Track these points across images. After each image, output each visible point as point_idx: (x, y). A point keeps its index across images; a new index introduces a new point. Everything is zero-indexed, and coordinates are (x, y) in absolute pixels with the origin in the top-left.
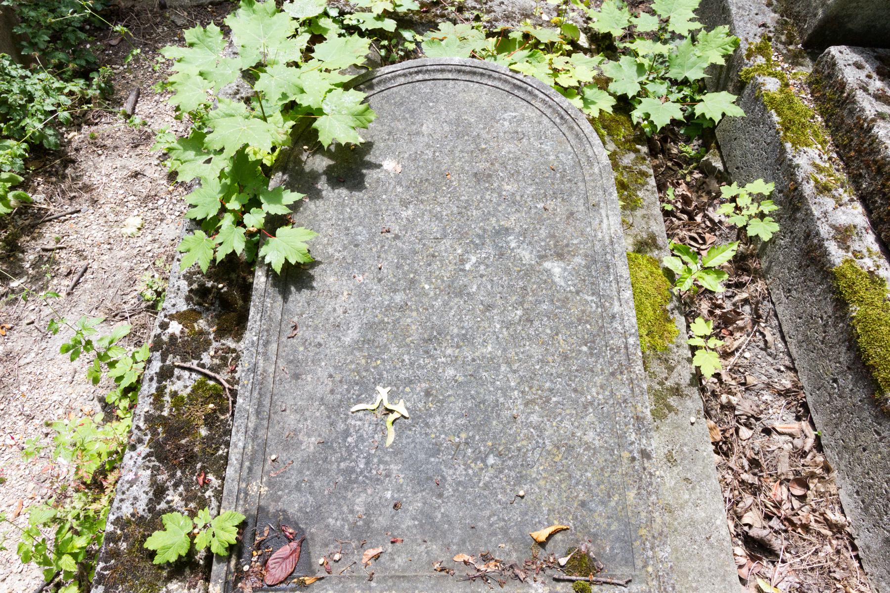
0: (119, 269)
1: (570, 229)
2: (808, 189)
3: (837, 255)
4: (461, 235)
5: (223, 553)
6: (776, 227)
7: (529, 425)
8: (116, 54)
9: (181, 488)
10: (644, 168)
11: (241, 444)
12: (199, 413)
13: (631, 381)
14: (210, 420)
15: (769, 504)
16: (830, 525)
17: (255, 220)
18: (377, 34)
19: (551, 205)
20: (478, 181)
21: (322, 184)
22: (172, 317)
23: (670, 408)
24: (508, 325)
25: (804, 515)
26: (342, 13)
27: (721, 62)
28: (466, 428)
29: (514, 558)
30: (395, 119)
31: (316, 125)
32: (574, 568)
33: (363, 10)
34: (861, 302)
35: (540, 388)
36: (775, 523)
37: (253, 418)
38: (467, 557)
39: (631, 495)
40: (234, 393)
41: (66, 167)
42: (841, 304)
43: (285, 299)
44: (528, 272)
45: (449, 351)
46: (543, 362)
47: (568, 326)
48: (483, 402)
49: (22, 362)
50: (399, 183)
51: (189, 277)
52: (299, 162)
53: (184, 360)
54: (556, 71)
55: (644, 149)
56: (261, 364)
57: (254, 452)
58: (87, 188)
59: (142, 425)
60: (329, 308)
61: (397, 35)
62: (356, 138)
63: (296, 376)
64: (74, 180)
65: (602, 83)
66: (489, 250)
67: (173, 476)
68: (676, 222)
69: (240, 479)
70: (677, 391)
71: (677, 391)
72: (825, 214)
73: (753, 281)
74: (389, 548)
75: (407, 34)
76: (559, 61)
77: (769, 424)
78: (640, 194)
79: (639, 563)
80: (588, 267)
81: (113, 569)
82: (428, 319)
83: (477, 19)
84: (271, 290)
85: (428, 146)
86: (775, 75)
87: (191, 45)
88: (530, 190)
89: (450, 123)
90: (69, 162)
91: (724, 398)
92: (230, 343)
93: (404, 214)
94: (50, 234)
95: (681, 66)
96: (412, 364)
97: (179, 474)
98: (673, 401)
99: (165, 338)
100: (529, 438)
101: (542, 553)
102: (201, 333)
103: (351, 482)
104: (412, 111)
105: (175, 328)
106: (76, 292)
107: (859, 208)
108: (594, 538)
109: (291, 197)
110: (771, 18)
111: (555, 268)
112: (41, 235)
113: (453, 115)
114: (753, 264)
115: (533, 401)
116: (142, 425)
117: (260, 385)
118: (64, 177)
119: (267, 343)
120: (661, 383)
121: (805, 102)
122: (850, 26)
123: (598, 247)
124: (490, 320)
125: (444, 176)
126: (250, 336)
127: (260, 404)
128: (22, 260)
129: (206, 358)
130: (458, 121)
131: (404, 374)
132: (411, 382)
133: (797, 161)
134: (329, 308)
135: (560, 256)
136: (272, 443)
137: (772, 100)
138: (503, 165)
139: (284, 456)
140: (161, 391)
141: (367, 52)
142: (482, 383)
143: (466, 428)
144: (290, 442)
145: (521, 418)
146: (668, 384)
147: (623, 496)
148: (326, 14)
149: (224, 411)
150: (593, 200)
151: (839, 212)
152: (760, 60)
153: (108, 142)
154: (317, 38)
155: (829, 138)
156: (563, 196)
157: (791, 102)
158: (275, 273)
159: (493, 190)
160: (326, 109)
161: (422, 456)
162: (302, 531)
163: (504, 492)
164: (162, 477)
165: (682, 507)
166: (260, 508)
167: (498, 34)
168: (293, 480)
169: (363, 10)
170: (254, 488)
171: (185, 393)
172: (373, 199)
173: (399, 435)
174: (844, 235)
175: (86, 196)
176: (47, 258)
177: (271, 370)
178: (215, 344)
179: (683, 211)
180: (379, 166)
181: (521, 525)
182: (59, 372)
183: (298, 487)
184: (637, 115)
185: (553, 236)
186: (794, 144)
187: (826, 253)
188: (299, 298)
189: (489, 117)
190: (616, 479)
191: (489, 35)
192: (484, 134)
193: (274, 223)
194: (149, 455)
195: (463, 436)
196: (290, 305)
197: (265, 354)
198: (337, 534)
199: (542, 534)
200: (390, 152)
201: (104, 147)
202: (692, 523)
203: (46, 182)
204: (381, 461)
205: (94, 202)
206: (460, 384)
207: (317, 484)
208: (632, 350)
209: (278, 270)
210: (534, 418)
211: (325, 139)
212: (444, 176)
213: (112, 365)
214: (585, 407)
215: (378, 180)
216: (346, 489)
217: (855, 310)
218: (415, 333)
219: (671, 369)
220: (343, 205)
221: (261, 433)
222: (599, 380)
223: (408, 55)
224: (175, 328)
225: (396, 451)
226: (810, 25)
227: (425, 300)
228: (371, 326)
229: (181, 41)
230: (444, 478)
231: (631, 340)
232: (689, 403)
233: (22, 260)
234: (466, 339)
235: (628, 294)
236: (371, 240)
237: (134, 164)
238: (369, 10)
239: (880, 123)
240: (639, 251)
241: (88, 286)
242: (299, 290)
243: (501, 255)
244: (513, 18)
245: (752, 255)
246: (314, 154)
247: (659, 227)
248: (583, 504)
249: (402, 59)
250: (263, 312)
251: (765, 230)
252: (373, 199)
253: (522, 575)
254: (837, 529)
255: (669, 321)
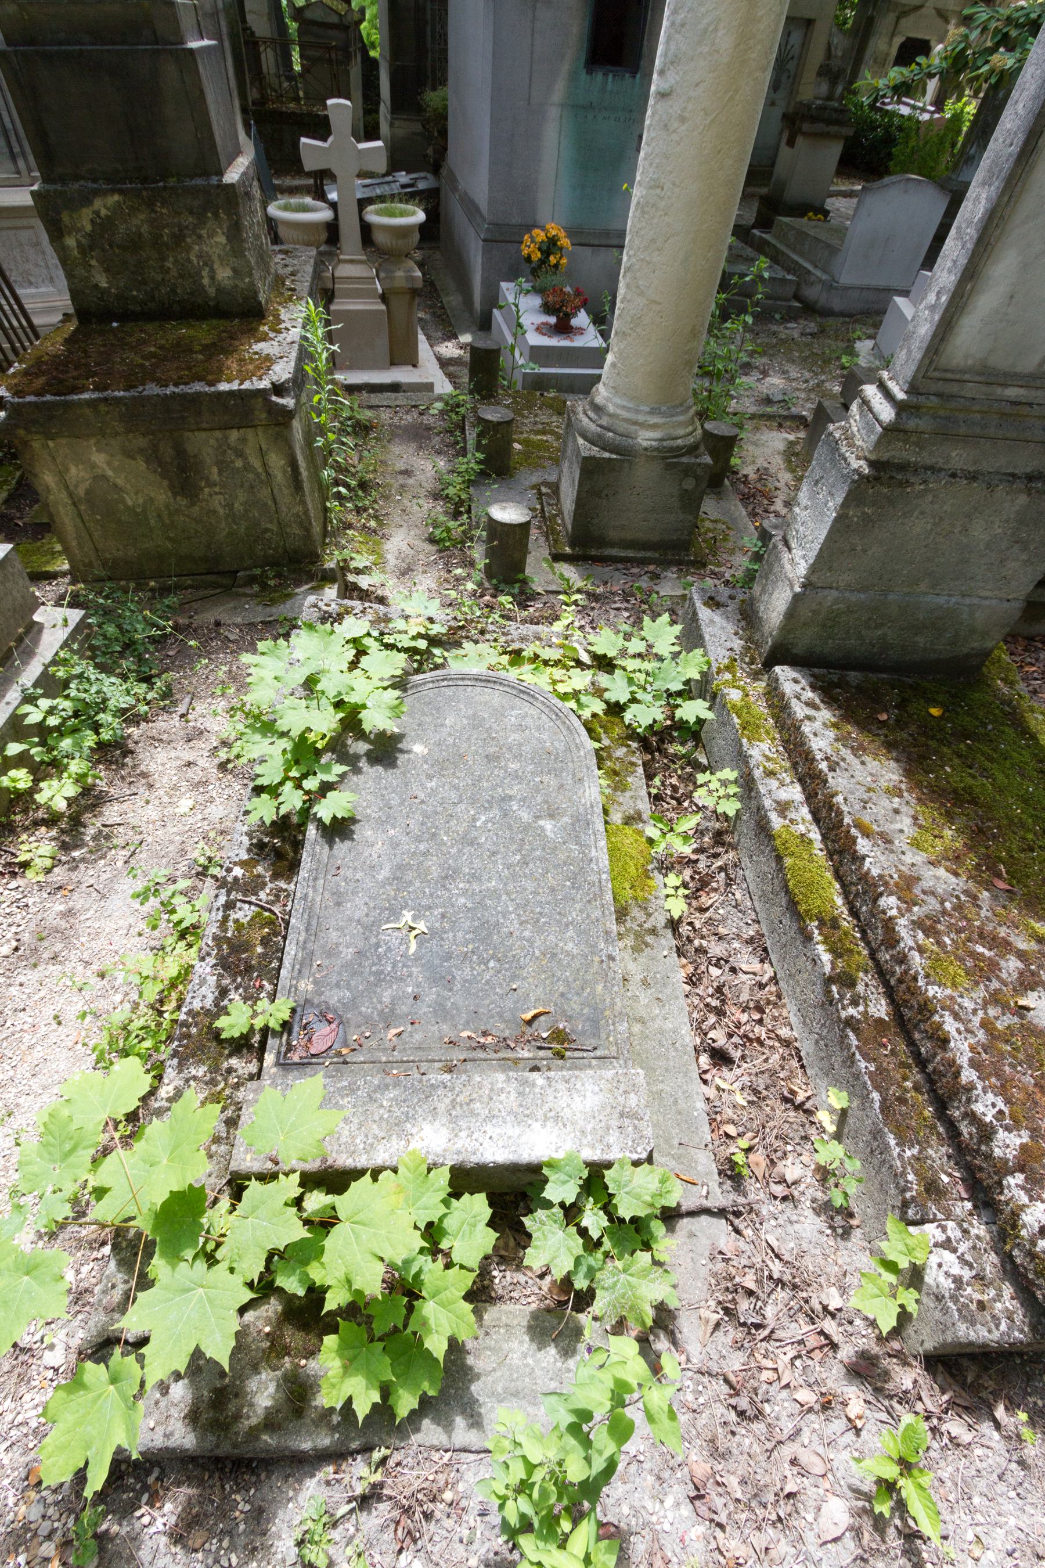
0: (172, 842)
1: (561, 797)
2: (758, 773)
3: (776, 822)
4: (473, 801)
5: (278, 1028)
6: (739, 805)
7: (524, 938)
8: (173, 663)
9: (241, 990)
10: (634, 759)
11: (293, 952)
12: (256, 936)
13: (603, 906)
14: (265, 941)
15: (731, 1025)
16: (779, 1038)
17: (311, 784)
18: (412, 651)
19: (546, 779)
20: (489, 761)
21: (363, 763)
22: (235, 864)
23: (647, 945)
24: (509, 866)
25: (760, 1032)
26: (382, 634)
27: (698, 677)
28: (473, 941)
29: (507, 1033)
30: (424, 714)
31: (360, 716)
32: (554, 1039)
33: (400, 632)
34: (792, 854)
35: (532, 912)
36: (736, 1039)
37: (303, 934)
38: (469, 1033)
39: (599, 988)
40: (287, 923)
41: (125, 757)
42: (779, 859)
43: (331, 848)
44: (526, 828)
45: (461, 885)
46: (535, 893)
47: (556, 867)
48: (487, 922)
49: (82, 918)
50: (426, 762)
51: (250, 834)
52: (346, 746)
53: (245, 895)
54: (554, 682)
55: (634, 745)
56: (311, 894)
57: (303, 959)
58: (144, 775)
59: (210, 942)
60: (367, 854)
61: (428, 651)
62: (392, 727)
63: (338, 904)
64: (135, 767)
65: (599, 692)
66: (496, 812)
67: (234, 981)
68: (666, 806)
69: (292, 978)
70: (653, 932)
71: (653, 932)
72: (770, 792)
73: (726, 852)
74: (409, 1028)
75: (437, 651)
76: (558, 673)
77: (735, 965)
78: (629, 779)
79: (603, 1036)
80: (573, 824)
81: (186, 1047)
82: (446, 862)
83: (495, 640)
84: (320, 840)
85: (450, 735)
86: (738, 688)
87: (263, 654)
88: (530, 768)
89: (468, 718)
90: (128, 752)
91: (697, 942)
92: (282, 884)
93: (429, 785)
94: (111, 813)
95: (664, 679)
96: (431, 895)
97: (239, 980)
98: (649, 939)
99: (230, 879)
100: (522, 948)
101: (529, 1030)
102: (259, 876)
103: (380, 980)
104: (438, 709)
105: (238, 872)
106: (133, 861)
107: (798, 788)
108: (569, 1019)
109: (339, 769)
110: (738, 644)
111: (548, 825)
112: (101, 814)
113: (470, 712)
114: (728, 839)
115: (526, 922)
116: (210, 942)
117: (309, 909)
118: (124, 765)
119: (315, 879)
120: (641, 926)
121: (761, 708)
122: (795, 651)
123: (581, 810)
124: (495, 863)
125: (462, 757)
126: (303, 873)
127: (309, 924)
128: (84, 834)
129: (262, 895)
130: (474, 717)
131: (425, 902)
132: (430, 908)
133: (750, 752)
134: (367, 854)
135: (552, 816)
136: (318, 953)
137: (734, 706)
138: (510, 749)
139: (326, 962)
140: (226, 918)
141: (404, 665)
142: (486, 908)
143: (473, 941)
144: (331, 953)
145: (516, 933)
146: (646, 926)
147: (593, 989)
148: (369, 634)
149: (276, 934)
150: (579, 775)
151: (781, 791)
152: (728, 676)
153: (165, 737)
154: (361, 653)
155: (777, 736)
156: (556, 773)
157: (749, 708)
158: (324, 824)
159: (501, 768)
160: (369, 704)
161: (437, 962)
162: (341, 1017)
163: (501, 987)
164: (226, 982)
165: (653, 1019)
166: (306, 1000)
167: (511, 653)
168: (334, 979)
169: (400, 632)
170: (302, 985)
171: (245, 921)
172: (404, 774)
173: (420, 946)
174: (783, 808)
175: (144, 781)
176: (104, 836)
177: (318, 899)
178: (270, 885)
179: (672, 798)
180: (409, 752)
181: (513, 1011)
182: (115, 927)
183: (338, 985)
184: (628, 716)
185: (546, 802)
186: (749, 739)
187: (769, 822)
188: (342, 847)
189: (499, 714)
190: (589, 977)
191: (505, 653)
192: (494, 726)
193: (326, 788)
194: (215, 965)
195: (470, 947)
196: (335, 851)
197: (314, 887)
198: (368, 1020)
199: (528, 1016)
200: (419, 738)
201: (161, 740)
202: (662, 1032)
203: (107, 769)
204: (404, 966)
205: (151, 786)
206: (469, 909)
207: (353, 983)
208: (604, 883)
209: (327, 821)
210: (527, 934)
211: (367, 726)
212: (462, 757)
213: (173, 911)
214: (567, 925)
215: (409, 760)
216: (376, 985)
217: (788, 861)
218: (435, 872)
219: (649, 915)
220: (380, 778)
221: (309, 945)
222: (578, 906)
223: (437, 667)
224: (238, 872)
225: (417, 958)
226: (766, 649)
227: (444, 848)
228: (399, 867)
229: (254, 651)
230: (454, 977)
231: (604, 876)
232: (663, 941)
233: (84, 834)
234: (475, 877)
235: (603, 843)
236: (402, 803)
237: (188, 756)
238: (406, 632)
239: (807, 722)
240: (626, 824)
241: (143, 856)
242: (342, 841)
243: (505, 815)
244: (527, 640)
245: (727, 832)
246: (357, 740)
247: (645, 806)
248: (562, 995)
249: (431, 670)
250: (313, 856)
251: (730, 808)
252: (404, 774)
253: (512, 1045)
254: (787, 1043)
255: (649, 878)
